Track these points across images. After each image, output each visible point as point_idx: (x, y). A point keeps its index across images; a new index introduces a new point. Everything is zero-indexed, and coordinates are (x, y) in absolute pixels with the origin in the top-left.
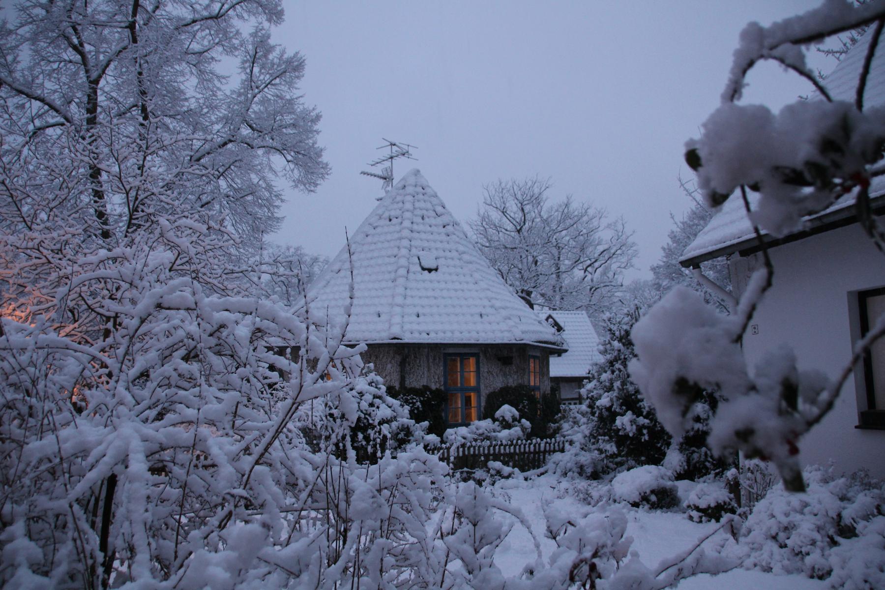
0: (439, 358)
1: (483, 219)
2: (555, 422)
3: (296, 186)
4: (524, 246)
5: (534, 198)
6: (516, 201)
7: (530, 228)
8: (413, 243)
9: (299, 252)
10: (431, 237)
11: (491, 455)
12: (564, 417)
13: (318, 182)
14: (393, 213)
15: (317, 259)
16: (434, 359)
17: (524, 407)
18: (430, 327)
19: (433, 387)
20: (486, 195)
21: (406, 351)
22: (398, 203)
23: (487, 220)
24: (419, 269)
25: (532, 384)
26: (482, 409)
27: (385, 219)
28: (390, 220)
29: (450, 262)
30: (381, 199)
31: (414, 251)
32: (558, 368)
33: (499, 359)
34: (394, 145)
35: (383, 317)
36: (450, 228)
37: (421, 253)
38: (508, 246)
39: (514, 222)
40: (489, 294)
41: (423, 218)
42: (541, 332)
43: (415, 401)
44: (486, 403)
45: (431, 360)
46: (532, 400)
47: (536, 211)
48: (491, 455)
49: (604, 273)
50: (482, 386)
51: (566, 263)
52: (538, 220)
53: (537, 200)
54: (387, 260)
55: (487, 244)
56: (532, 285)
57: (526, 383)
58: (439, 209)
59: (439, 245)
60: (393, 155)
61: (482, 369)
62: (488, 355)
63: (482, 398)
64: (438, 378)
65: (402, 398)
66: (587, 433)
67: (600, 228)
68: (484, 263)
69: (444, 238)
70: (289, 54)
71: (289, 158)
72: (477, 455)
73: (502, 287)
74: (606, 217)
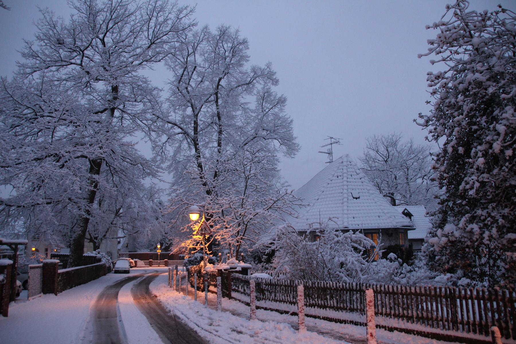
2: (412, 260)
3: (285, 156)
8: (348, 187)
10: (355, 184)
12: (415, 258)
13: (296, 153)
14: (339, 174)
17: (399, 254)
18: (359, 223)
20: (368, 143)
22: (340, 169)
25: (401, 244)
29: (364, 194)
31: (349, 190)
32: (411, 235)
37: (352, 191)
41: (351, 176)
46: (401, 250)
53: (394, 144)
55: (369, 169)
57: (399, 244)
59: (359, 187)
66: (425, 263)
69: (361, 184)
70: (279, 95)
74: (433, 149)
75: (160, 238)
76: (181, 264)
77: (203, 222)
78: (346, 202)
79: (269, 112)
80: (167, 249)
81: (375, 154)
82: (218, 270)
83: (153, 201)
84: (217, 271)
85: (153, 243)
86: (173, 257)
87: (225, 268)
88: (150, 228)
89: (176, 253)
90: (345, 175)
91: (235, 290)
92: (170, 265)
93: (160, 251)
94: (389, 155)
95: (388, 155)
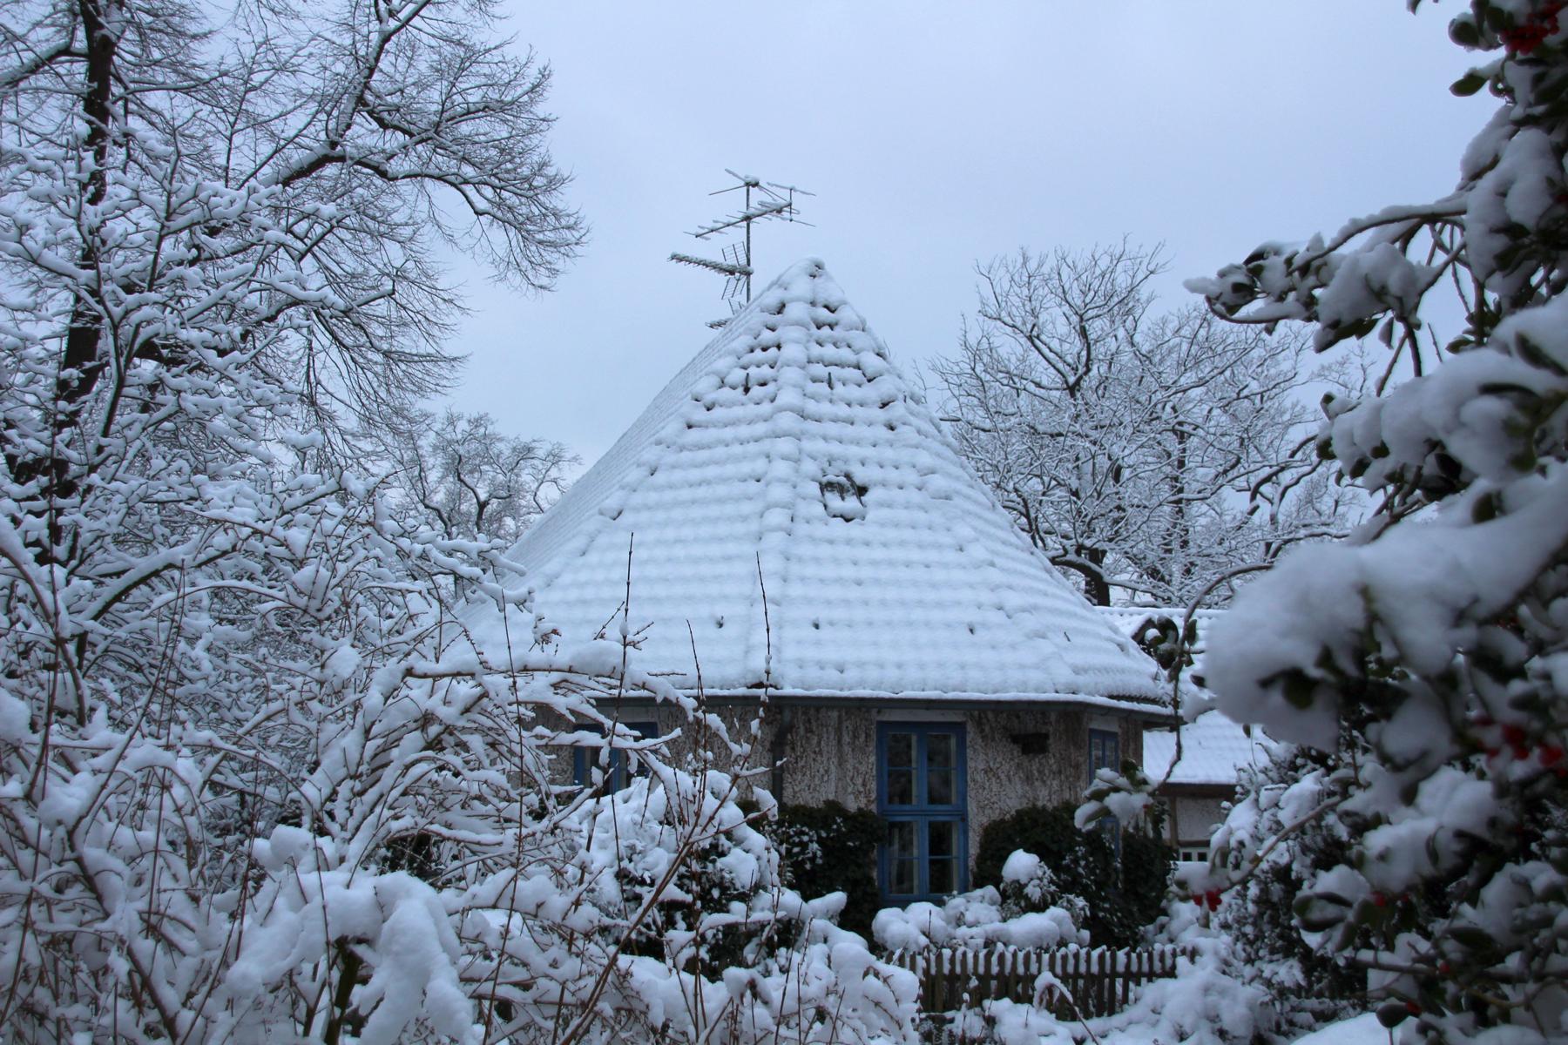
0: (867, 736)
1: (976, 356)
3: (503, 279)
4: (1087, 429)
5: (1116, 300)
6: (1066, 308)
7: (1103, 382)
9: (482, 430)
11: (994, 978)
13: (559, 265)
15: (529, 450)
16: (855, 737)
18: (849, 655)
19: (852, 805)
20: (987, 291)
21: (787, 715)
23: (986, 359)
26: (971, 863)
28: (747, 390)
30: (720, 324)
33: (1015, 739)
34: (756, 184)
36: (897, 410)
38: (1041, 428)
39: (1060, 365)
40: (995, 575)
42: (1123, 671)
43: (806, 838)
44: (982, 846)
45: (846, 739)
47: (1121, 333)
48: (994, 978)
49: (1309, 500)
51: (1200, 473)
52: (1126, 357)
53: (1124, 305)
54: (737, 488)
55: (988, 424)
56: (1108, 533)
58: (871, 361)
61: (971, 764)
62: (987, 729)
63: (971, 834)
64: (864, 785)
65: (774, 832)
67: (1300, 379)
68: (982, 499)
71: (482, 205)
72: (958, 977)
73: (1026, 556)
79: (416, 21)
81: (1019, 351)
94: (1088, 359)
95: (1084, 359)
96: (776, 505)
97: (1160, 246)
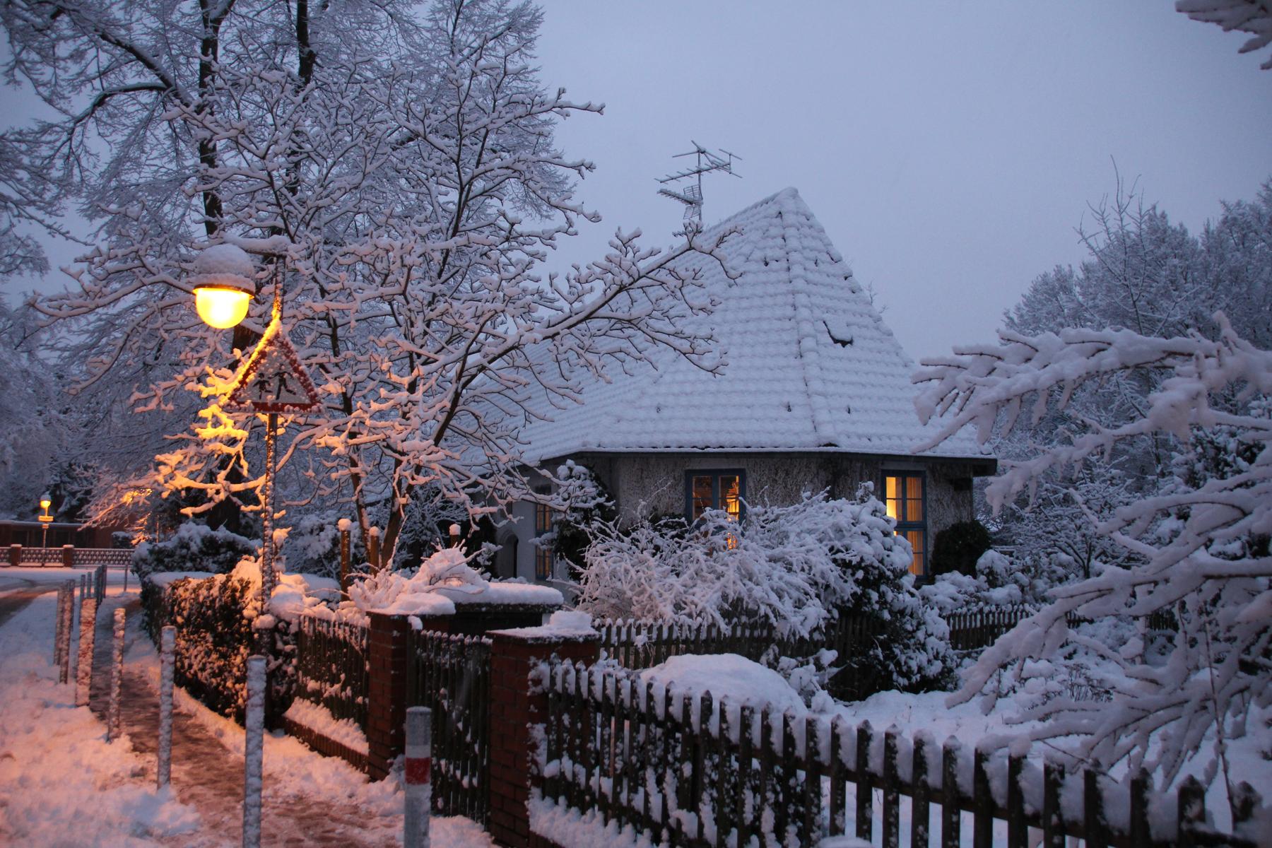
10: (832, 293)
22: (774, 238)
24: (831, 341)
26: (930, 556)
27: (757, 261)
28: (767, 264)
33: (951, 482)
35: (797, 411)
37: (826, 316)
50: (930, 522)
54: (777, 324)
60: (703, 166)
61: (929, 496)
75: (50, 479)
76: (121, 561)
77: (270, 343)
78: (812, 350)
80: (72, 514)
82: (378, 619)
83: (30, 352)
84: (367, 621)
85: (28, 495)
86: (91, 538)
87: (426, 610)
88: (12, 436)
89: (104, 523)
90: (794, 256)
91: (556, 788)
92: (82, 562)
93: (51, 518)
96: (807, 336)
97: (1224, 203)
